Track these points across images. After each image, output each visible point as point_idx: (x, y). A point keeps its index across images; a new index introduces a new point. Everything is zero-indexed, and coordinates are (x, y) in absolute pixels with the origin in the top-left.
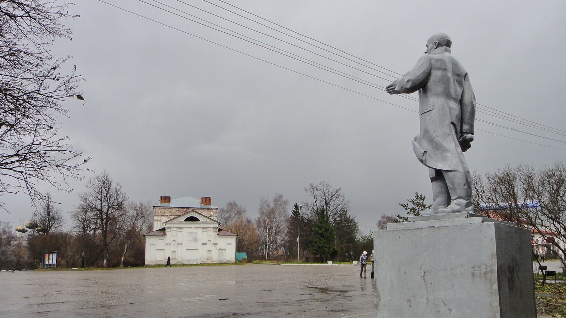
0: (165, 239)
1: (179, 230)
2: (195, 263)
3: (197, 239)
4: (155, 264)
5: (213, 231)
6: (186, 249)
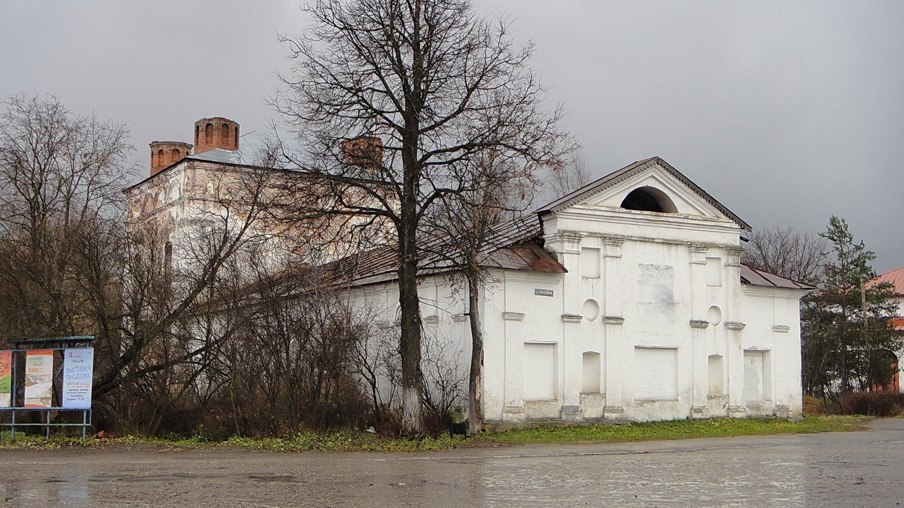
0: (556, 289)
1: (610, 250)
2: (670, 418)
3: (671, 297)
4: (523, 416)
5: (724, 261)
6: (636, 347)
